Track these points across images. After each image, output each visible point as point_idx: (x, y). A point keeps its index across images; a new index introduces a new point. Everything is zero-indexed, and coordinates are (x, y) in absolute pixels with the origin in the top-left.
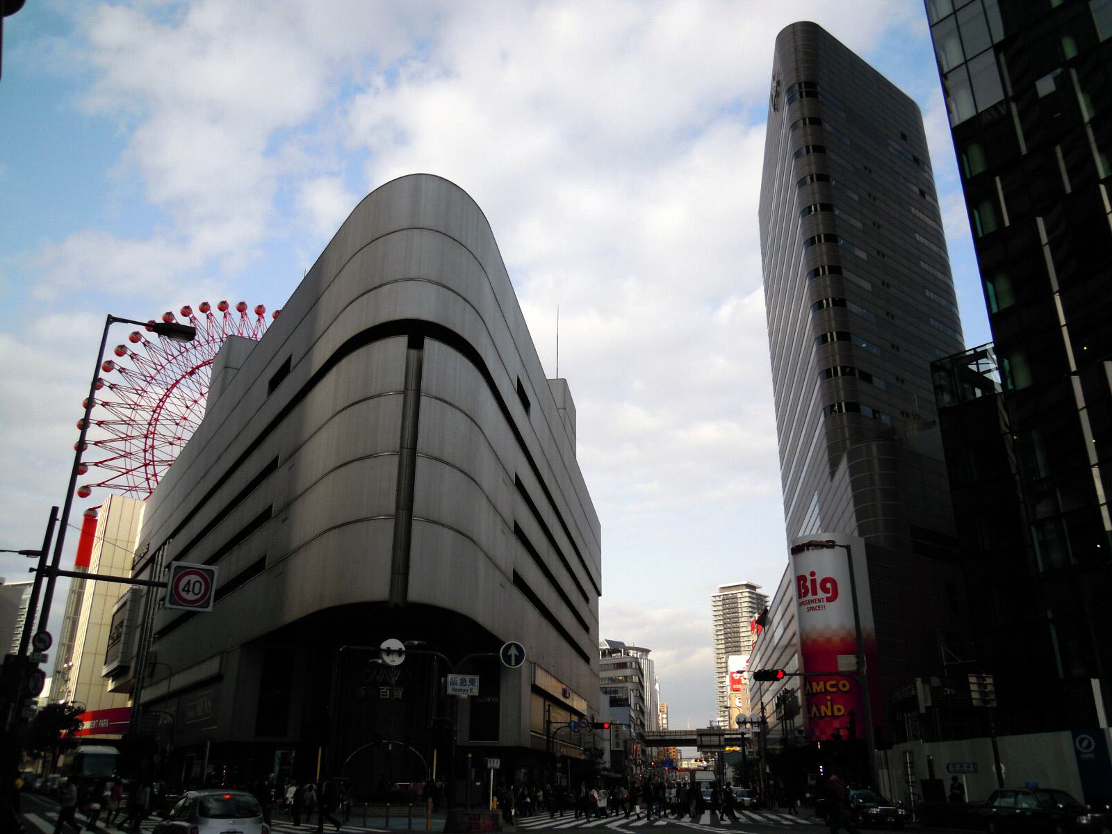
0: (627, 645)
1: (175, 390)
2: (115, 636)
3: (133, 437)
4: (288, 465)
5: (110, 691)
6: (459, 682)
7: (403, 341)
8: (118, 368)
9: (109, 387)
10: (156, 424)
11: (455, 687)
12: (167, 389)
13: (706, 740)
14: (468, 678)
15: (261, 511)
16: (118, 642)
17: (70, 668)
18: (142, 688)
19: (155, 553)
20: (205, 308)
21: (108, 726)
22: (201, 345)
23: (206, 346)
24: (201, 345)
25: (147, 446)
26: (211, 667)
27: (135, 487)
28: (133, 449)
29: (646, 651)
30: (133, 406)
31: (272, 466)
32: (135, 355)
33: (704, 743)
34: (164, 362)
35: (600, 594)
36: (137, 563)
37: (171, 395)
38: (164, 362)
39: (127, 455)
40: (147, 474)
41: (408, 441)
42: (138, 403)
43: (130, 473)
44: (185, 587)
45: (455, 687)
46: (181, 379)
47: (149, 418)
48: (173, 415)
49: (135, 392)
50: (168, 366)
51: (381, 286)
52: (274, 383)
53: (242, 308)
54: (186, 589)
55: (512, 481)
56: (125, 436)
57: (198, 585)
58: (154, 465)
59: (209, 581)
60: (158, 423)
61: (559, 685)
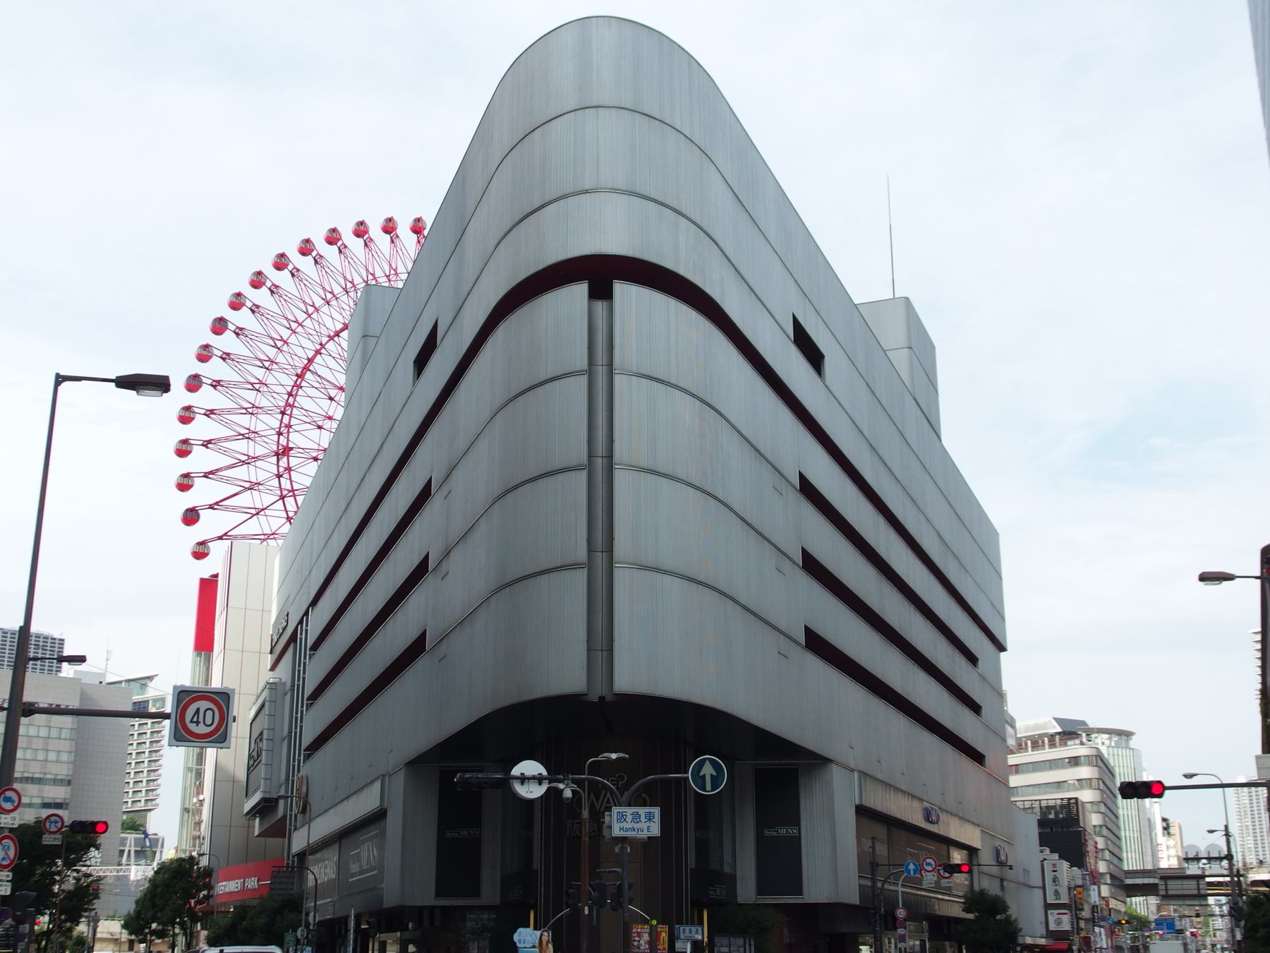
0: (1091, 725)
1: (308, 375)
2: (255, 754)
3: (256, 458)
4: (445, 490)
5: (257, 836)
6: (629, 818)
7: (579, 291)
8: (220, 354)
9: (211, 385)
10: (288, 432)
11: (625, 825)
12: (297, 375)
13: (1174, 887)
14: (642, 811)
15: (416, 561)
16: (260, 762)
17: (201, 802)
18: (296, 829)
19: (296, 629)
20: (333, 238)
21: (256, 886)
22: (337, 298)
23: (345, 298)
24: (337, 298)
25: (281, 469)
26: (367, 802)
27: (273, 534)
28: (262, 476)
29: (1125, 735)
30: (250, 410)
31: (424, 495)
32: (241, 329)
33: (1170, 892)
34: (286, 333)
35: (1002, 648)
36: (276, 643)
37: (304, 384)
38: (286, 333)
39: (253, 486)
40: (287, 512)
41: (600, 449)
42: (257, 405)
43: (262, 513)
44: (193, 718)
45: (625, 825)
46: (314, 356)
47: (277, 424)
48: (312, 414)
49: (250, 387)
50: (293, 340)
51: (542, 207)
52: (421, 362)
53: (389, 228)
54: (195, 719)
55: (794, 487)
56: (246, 458)
57: (209, 713)
58: (294, 496)
59: (225, 709)
60: (291, 430)
61: (916, 804)
